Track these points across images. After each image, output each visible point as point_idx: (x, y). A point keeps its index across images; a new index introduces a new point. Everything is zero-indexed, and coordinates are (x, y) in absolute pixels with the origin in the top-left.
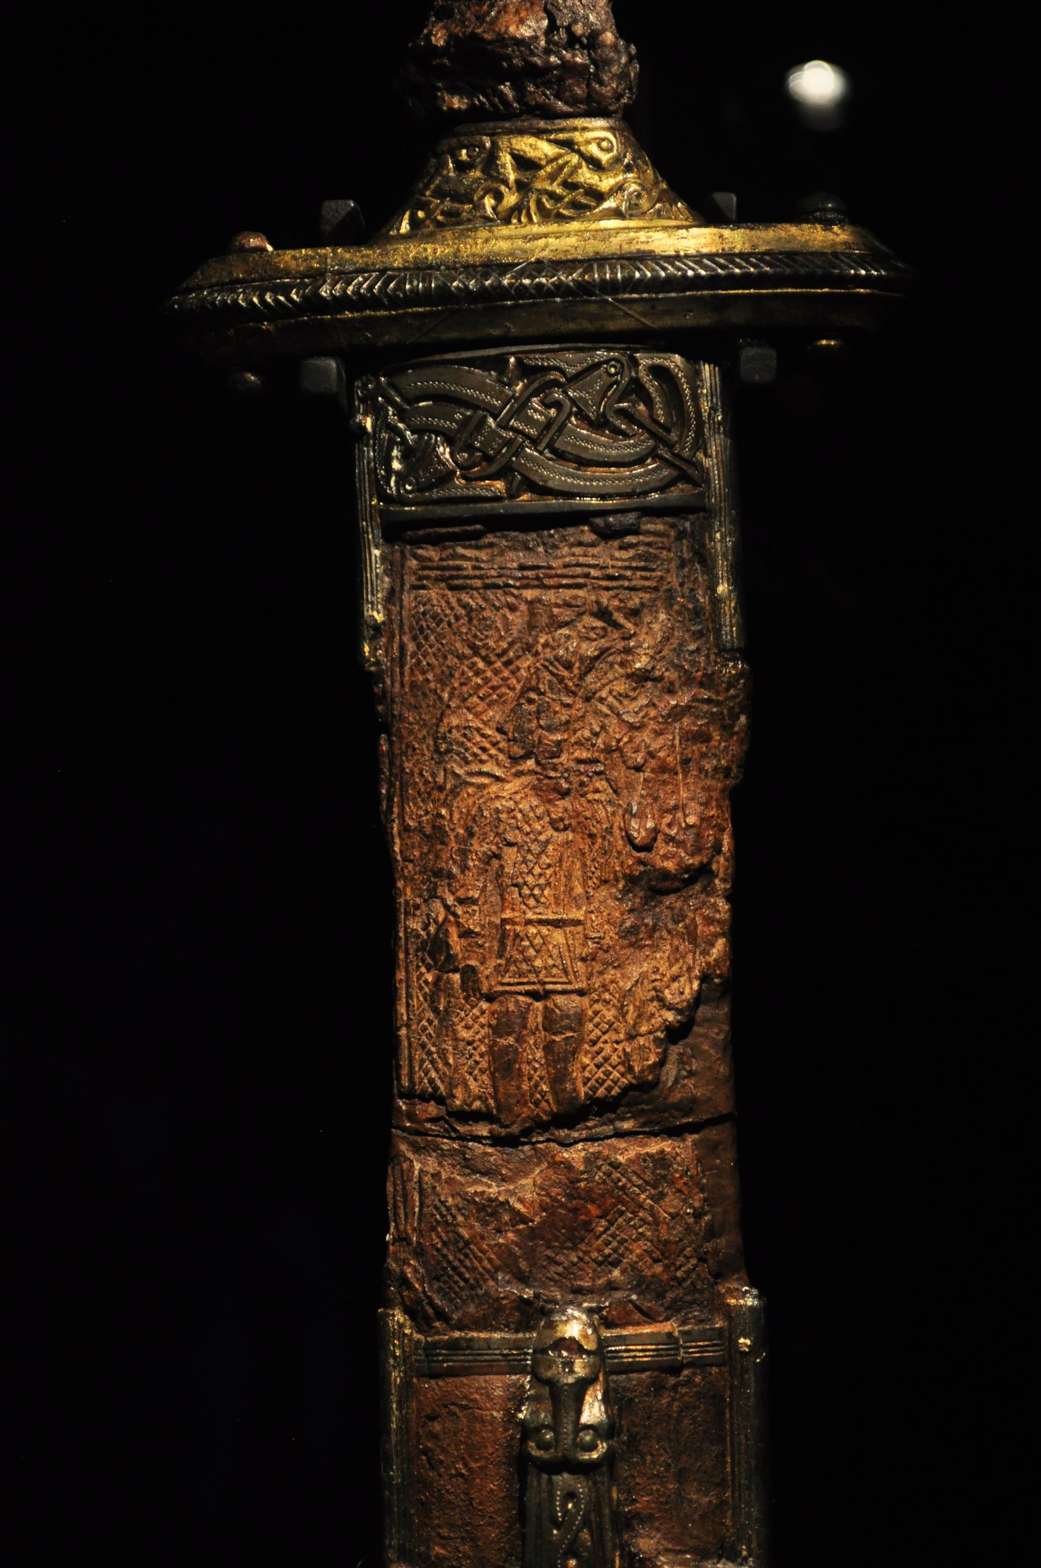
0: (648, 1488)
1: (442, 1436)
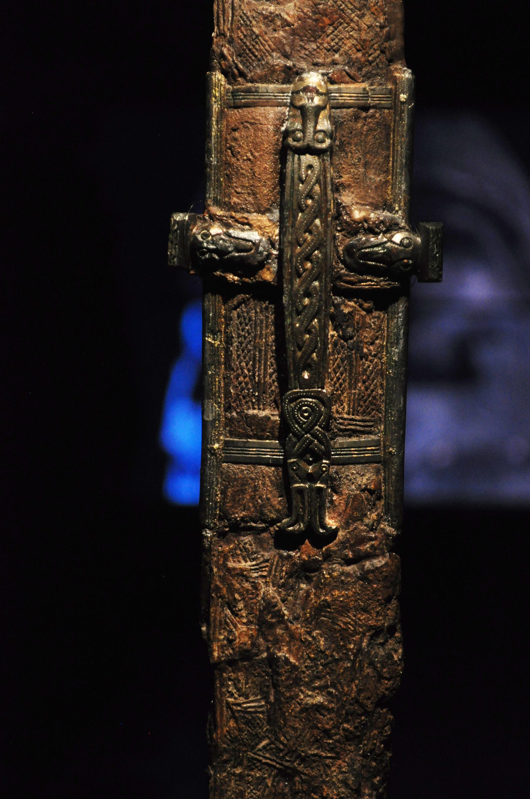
0: (349, 170)
1: (240, 139)
